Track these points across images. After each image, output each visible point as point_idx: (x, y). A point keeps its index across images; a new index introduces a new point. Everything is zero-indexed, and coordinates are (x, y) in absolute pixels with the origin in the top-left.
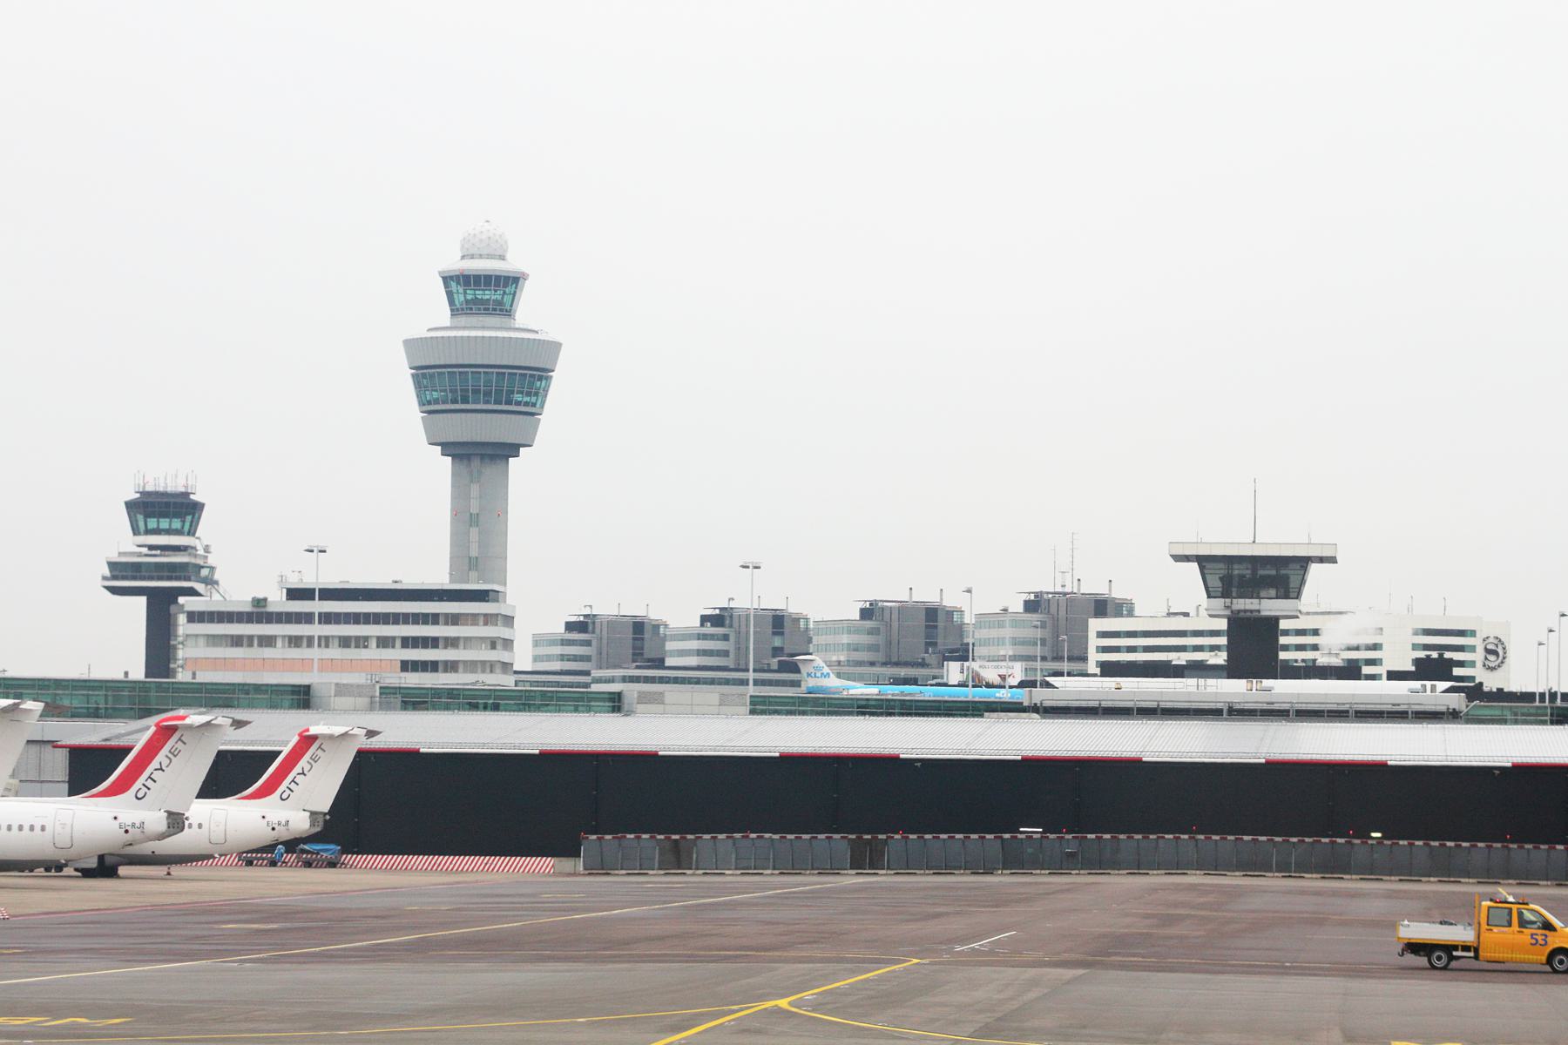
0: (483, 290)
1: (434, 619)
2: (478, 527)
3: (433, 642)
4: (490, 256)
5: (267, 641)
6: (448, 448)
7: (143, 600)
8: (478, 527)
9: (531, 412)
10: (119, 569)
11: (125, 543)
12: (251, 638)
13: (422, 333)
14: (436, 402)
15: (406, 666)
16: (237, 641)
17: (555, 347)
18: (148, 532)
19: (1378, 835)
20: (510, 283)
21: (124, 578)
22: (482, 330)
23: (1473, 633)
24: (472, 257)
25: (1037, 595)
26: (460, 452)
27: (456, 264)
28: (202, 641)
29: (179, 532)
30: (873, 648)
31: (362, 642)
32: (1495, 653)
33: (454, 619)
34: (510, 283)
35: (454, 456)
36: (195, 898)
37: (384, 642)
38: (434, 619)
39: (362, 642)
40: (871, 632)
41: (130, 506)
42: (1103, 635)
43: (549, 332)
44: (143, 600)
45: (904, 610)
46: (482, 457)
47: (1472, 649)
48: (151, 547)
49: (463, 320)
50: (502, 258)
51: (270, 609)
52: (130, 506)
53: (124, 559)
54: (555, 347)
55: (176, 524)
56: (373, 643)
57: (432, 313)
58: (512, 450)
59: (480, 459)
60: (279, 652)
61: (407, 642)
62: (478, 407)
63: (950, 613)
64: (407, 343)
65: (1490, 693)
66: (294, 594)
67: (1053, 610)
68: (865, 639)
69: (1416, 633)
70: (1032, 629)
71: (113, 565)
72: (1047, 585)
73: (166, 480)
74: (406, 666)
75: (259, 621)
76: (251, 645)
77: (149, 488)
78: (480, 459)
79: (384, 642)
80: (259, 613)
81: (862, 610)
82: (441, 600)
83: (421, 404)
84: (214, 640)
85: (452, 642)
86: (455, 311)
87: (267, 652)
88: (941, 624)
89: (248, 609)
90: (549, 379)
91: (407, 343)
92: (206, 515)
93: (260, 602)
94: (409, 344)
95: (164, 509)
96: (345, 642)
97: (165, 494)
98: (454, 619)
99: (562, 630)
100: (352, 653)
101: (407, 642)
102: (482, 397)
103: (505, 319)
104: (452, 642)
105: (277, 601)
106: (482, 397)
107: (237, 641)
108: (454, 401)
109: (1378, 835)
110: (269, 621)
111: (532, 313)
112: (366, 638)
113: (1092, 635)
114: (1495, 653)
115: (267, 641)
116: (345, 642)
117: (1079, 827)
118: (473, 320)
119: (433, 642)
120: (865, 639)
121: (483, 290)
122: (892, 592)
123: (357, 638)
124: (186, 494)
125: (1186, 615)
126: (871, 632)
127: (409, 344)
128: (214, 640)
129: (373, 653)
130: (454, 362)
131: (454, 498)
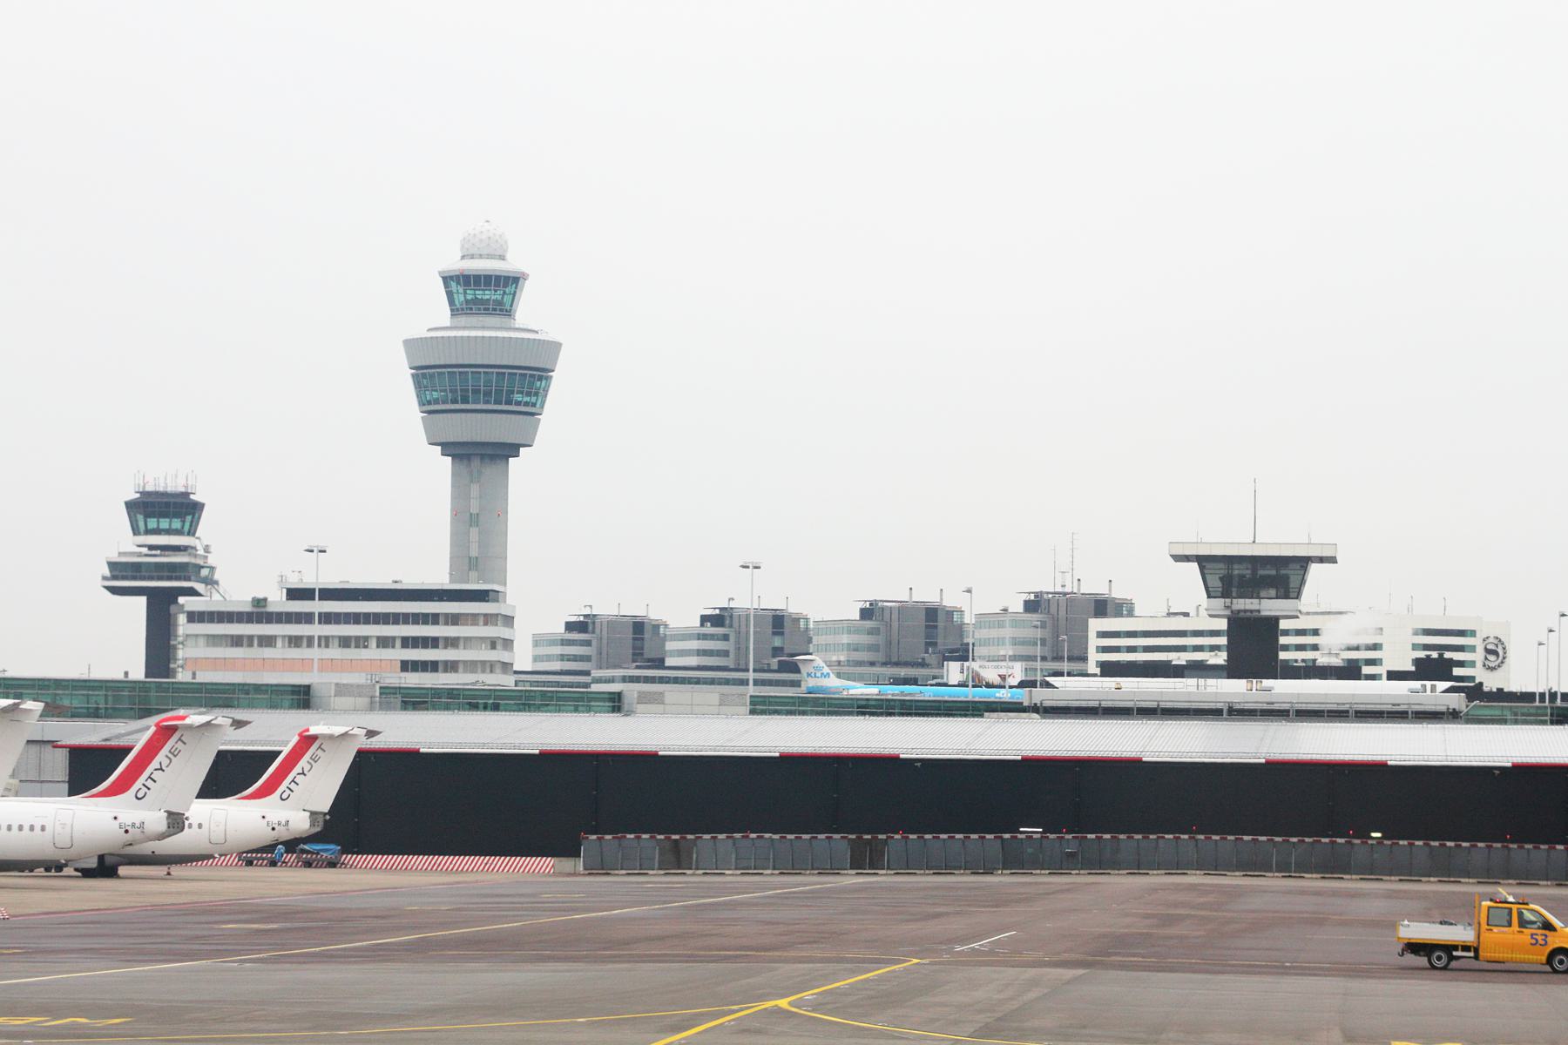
0: (483, 290)
1: (434, 619)
2: (478, 527)
3: (433, 642)
4: (490, 256)
5: (267, 641)
6: (448, 448)
7: (143, 600)
8: (478, 527)
9: (531, 412)
10: (119, 569)
11: (125, 543)
12: (251, 638)
13: (422, 333)
14: (436, 402)
15: (406, 666)
16: (237, 641)
17: (555, 347)
18: (148, 532)
19: (1378, 835)
20: (510, 283)
21: (124, 578)
22: (482, 330)
23: (1473, 633)
24: (472, 257)
25: (1037, 595)
26: (460, 452)
27: (456, 264)
28: (202, 641)
29: (179, 532)
30: (873, 648)
31: (362, 642)
32: (1495, 653)
33: (454, 619)
34: (510, 283)
35: (454, 456)
36: (195, 898)
37: (384, 642)
38: (434, 619)
39: (362, 642)
40: (871, 632)
41: (130, 506)
42: (1103, 635)
43: (549, 332)
44: (143, 600)
45: (904, 610)
46: (482, 457)
47: (1472, 649)
48: (151, 547)
49: (463, 320)
50: (502, 258)
51: (270, 609)
52: (130, 506)
53: (124, 559)
54: (555, 347)
55: (176, 524)
56: (373, 643)
57: (432, 313)
58: (512, 450)
59: (480, 459)
60: (279, 652)
61: (407, 642)
62: (478, 407)
63: (950, 613)
64: (407, 343)
65: (1490, 693)
66: (294, 594)
67: (1053, 610)
68: (865, 639)
69: (1416, 633)
70: (1032, 629)
71: (113, 565)
72: (1047, 585)
73: (166, 480)
74: (406, 666)
75: (259, 621)
76: (251, 645)
77: (149, 488)
78: (480, 459)
79: (384, 642)
80: (259, 613)
81: (862, 610)
82: (441, 600)
83: (421, 404)
84: (214, 640)
85: (452, 642)
86: (455, 311)
87: (267, 652)
88: (941, 624)
89: (248, 609)
90: (549, 379)
91: (407, 343)
92: (206, 515)
93: (260, 602)
94: (409, 344)
95: (164, 509)
96: (345, 642)
97: (165, 494)
98: (454, 619)
99: (562, 630)
100: (352, 653)
101: (407, 642)
102: (482, 397)
103: (505, 319)
104: (452, 642)
105: (277, 601)
106: (482, 397)
107: (237, 641)
108: (454, 401)
109: (1378, 835)
110: (269, 621)
111: (532, 313)
112: (366, 638)
113: (1092, 635)
114: (1495, 653)
115: (267, 641)
116: (345, 642)
117: (1079, 827)
118: (473, 320)
119: (433, 642)
120: (865, 639)
121: (483, 290)
122: (892, 592)
123: (357, 638)
124: (186, 494)
125: (1186, 615)
126: (871, 632)
127: (409, 344)
128: (214, 640)
129: (373, 653)
130: (454, 362)
131: (454, 498)
